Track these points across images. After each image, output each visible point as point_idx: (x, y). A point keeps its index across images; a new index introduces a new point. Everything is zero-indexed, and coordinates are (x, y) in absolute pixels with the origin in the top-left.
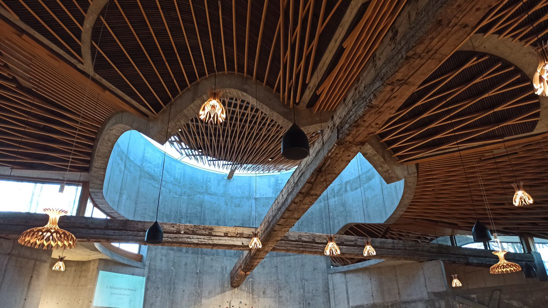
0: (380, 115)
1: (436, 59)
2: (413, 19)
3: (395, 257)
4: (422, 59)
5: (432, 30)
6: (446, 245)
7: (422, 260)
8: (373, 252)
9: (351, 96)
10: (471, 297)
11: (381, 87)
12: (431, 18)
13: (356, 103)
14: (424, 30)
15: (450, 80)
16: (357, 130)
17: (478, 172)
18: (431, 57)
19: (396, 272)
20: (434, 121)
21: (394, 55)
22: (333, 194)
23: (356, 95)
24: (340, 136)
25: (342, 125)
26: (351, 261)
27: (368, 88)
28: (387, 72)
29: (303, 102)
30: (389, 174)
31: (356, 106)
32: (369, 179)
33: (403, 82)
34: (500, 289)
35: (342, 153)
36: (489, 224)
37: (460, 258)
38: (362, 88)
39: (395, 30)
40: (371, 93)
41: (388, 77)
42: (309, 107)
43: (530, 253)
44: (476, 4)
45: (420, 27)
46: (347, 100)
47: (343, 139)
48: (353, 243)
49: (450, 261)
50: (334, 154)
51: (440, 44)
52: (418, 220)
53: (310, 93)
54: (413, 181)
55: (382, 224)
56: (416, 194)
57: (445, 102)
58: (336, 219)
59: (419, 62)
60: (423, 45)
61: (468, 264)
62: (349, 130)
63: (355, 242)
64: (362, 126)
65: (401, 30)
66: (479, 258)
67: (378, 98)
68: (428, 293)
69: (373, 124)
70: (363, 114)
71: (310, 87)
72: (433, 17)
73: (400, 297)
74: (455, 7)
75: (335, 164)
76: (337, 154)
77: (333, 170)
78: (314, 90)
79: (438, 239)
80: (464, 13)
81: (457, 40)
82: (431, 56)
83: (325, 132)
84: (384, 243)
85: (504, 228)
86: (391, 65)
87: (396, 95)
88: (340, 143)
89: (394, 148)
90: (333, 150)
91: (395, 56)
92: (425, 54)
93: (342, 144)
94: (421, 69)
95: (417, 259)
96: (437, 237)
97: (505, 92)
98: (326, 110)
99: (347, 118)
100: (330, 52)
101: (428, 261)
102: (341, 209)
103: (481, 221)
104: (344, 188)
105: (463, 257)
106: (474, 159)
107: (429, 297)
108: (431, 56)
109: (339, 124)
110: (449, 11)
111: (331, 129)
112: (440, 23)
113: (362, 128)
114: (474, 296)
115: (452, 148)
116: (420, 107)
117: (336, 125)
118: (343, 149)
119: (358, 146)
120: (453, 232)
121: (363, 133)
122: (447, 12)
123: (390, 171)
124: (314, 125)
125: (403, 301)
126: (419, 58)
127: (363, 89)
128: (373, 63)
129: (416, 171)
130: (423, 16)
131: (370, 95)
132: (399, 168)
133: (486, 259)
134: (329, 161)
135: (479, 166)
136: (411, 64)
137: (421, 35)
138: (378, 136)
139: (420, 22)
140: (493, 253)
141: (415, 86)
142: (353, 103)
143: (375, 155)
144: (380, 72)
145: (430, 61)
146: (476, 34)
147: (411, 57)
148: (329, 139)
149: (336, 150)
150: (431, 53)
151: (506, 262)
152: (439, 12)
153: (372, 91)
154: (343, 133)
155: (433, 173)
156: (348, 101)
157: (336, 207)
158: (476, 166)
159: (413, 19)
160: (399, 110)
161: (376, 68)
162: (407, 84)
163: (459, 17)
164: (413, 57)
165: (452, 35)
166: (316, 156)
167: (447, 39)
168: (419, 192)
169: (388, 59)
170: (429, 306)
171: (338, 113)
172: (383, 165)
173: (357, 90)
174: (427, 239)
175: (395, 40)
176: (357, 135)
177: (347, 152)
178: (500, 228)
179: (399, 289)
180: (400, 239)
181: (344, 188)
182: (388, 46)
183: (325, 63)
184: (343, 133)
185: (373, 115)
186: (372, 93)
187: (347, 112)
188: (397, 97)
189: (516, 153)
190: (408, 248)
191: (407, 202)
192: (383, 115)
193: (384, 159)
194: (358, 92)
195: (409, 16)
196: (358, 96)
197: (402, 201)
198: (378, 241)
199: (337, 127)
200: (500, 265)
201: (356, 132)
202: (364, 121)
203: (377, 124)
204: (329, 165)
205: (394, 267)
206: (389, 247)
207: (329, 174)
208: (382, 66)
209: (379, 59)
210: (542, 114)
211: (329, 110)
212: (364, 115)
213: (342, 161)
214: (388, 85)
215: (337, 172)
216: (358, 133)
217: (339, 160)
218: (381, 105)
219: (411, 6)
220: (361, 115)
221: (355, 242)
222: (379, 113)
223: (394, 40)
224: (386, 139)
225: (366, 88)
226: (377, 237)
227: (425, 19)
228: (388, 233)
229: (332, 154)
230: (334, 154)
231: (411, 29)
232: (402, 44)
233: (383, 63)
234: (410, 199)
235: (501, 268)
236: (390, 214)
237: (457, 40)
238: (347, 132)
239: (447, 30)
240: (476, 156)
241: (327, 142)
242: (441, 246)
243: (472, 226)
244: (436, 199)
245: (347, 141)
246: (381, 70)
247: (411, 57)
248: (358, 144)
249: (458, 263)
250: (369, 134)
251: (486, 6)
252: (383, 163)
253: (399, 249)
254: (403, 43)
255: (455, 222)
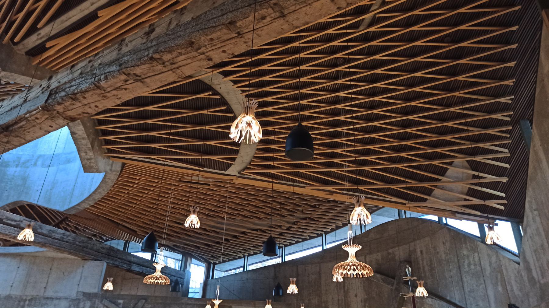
0: (104, 100)
1: (176, 74)
2: (171, 27)
3: (58, 249)
4: (165, 67)
5: (183, 46)
6: (117, 249)
7: (86, 258)
8: (31, 238)
9: (82, 66)
10: (118, 302)
11: (116, 72)
12: (186, 35)
13: (84, 76)
14: (176, 42)
15: (184, 101)
16: (72, 103)
17: (173, 189)
18: (173, 70)
19: (52, 265)
20: (156, 130)
21: (142, 49)
22: (17, 163)
23: (87, 67)
24: (50, 101)
25: (58, 91)
26: (3, 243)
27: (103, 66)
28: (128, 61)
29: (23, 45)
30: (90, 163)
31: (82, 78)
32: (69, 161)
33: (139, 79)
34: (145, 298)
35: (43, 119)
36: (161, 238)
37: (125, 263)
38: (96, 64)
39: (152, 28)
40: (103, 73)
41: (127, 66)
42: (29, 55)
43: (184, 272)
44: (224, 46)
45: (175, 38)
46: (75, 67)
47: (52, 106)
48: (14, 223)
49: (114, 264)
50: (33, 118)
51: (185, 62)
52: (101, 218)
53: (38, 39)
54: (113, 178)
55: (61, 211)
56: (110, 192)
57: (172, 117)
58: (6, 191)
59: (161, 68)
60: (171, 55)
61: (129, 271)
62: (62, 99)
63: (18, 223)
64: (80, 102)
65: (158, 30)
66: (142, 267)
67: (108, 82)
68: (78, 292)
69: (93, 105)
70: (86, 90)
71: (40, 34)
72: (189, 36)
73: (45, 292)
74: (208, 38)
75: (29, 128)
76: (37, 118)
77: (25, 134)
78: (44, 39)
79: (113, 241)
80: (213, 48)
81: (199, 67)
82: (173, 69)
83: (33, 90)
84: (53, 231)
85: (174, 245)
86: (135, 56)
87: (127, 88)
88: (46, 108)
89: (107, 139)
90: (34, 112)
91: (142, 50)
92: (169, 64)
93: (48, 111)
94: (160, 75)
95: (81, 256)
96: (113, 239)
97: (220, 131)
98: (49, 68)
99: (68, 85)
100: (82, 11)
101: (92, 260)
102: (20, 182)
103: (155, 233)
104: (34, 161)
105: (128, 263)
106: (174, 177)
107: (77, 296)
108: (173, 69)
109: (55, 88)
110: (202, 38)
111: (42, 89)
112: (191, 44)
113: (79, 103)
114: (121, 301)
115: (161, 160)
116: (149, 112)
117: (51, 88)
118: (47, 116)
119: (67, 120)
120: (130, 238)
121: (76, 109)
122: (201, 38)
123: (93, 161)
124: (25, 77)
125: (46, 297)
126: (162, 64)
127: (97, 65)
128: (119, 45)
129: (119, 169)
130: (181, 30)
131: (102, 75)
132: (104, 160)
133: (147, 269)
134: (24, 123)
135: (175, 185)
136: (153, 66)
137: (172, 46)
138: (96, 121)
139: (176, 33)
140: (153, 264)
141: (148, 88)
142: (81, 74)
143: (83, 139)
144: (122, 58)
145: (171, 72)
146: (230, 81)
147: (156, 59)
148: (35, 98)
149: (39, 114)
150: (174, 66)
151: (160, 274)
152: (194, 35)
153: (106, 72)
154: (54, 99)
155: (134, 177)
156: (77, 69)
157: (13, 179)
158: (173, 185)
159: (172, 27)
160: (124, 104)
161: (120, 52)
162: (142, 83)
163: (208, 49)
164: (158, 60)
165: (197, 61)
166: (9, 111)
167: (191, 61)
168: (114, 191)
169: (134, 50)
170: (72, 305)
171: (59, 76)
172: (88, 152)
173: (91, 63)
174: (102, 238)
175: (149, 36)
176: (69, 108)
177: (51, 122)
178: (171, 244)
179: (47, 282)
180: (74, 232)
181: (33, 161)
182: (139, 38)
183: (70, 18)
184: (54, 99)
185: (96, 95)
186: (105, 73)
187: (69, 80)
188: (128, 90)
189: (209, 185)
190: (77, 243)
191: (98, 197)
192: (107, 100)
193: (92, 147)
194: (91, 65)
195: (170, 23)
196: (89, 70)
197: (93, 194)
198: (47, 228)
199: (51, 91)
200: (154, 277)
201: (70, 104)
202: (84, 98)
203: (96, 106)
204: (21, 127)
205: (53, 259)
206: (56, 237)
207: (17, 136)
208: (126, 53)
209: (126, 45)
210: (237, 160)
211: (52, 70)
212: (86, 91)
213: (40, 129)
214: (123, 74)
215: (28, 138)
216: (72, 107)
217: (37, 127)
218: (109, 89)
219: (175, 15)
220: (83, 89)
221: (18, 223)
222: (103, 96)
223: (148, 36)
224: (103, 127)
225: (101, 66)
226: (49, 223)
227: (182, 33)
228: (64, 223)
229: (30, 117)
230: (33, 118)
231: (167, 34)
232: (153, 44)
233: (128, 50)
234: (102, 195)
235: (154, 279)
236: (74, 204)
237: (199, 67)
238: (60, 100)
239: (195, 54)
240: (177, 176)
241: (31, 101)
242: (111, 248)
243: (145, 235)
244: (127, 203)
245: (55, 110)
246: (123, 56)
247: (156, 59)
248: (67, 118)
249: (120, 268)
250: (84, 113)
251: (231, 52)
252: (89, 150)
253: (67, 242)
254: (154, 43)
255: (135, 228)
